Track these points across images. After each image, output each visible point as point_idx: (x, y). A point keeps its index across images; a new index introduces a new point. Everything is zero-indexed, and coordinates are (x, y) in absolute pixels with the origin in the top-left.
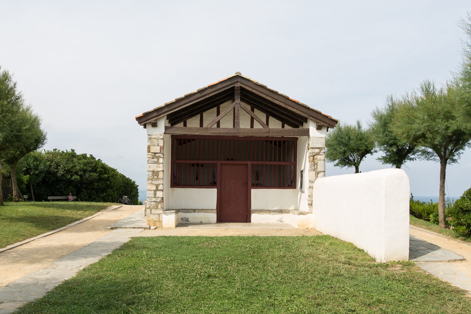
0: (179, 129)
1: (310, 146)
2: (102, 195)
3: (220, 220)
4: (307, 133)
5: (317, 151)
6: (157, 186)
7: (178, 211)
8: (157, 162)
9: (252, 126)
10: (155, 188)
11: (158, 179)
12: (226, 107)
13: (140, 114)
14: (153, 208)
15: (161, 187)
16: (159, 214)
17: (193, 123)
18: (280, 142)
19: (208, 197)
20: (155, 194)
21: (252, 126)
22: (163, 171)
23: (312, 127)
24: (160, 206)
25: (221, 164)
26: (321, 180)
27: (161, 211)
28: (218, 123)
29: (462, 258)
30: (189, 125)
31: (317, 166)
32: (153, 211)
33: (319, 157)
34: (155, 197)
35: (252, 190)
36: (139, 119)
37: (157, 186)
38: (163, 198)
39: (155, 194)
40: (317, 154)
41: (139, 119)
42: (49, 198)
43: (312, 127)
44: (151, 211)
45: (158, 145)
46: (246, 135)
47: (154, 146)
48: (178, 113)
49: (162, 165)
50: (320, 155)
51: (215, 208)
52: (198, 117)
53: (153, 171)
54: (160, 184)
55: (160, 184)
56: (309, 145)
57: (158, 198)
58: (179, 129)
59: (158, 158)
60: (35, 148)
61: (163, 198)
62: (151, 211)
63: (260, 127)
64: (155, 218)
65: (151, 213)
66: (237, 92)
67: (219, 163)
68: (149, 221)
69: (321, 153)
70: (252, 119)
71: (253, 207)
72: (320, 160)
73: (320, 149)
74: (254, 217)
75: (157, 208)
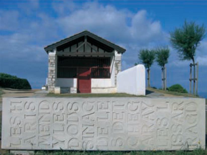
0: (61, 53)
1: (115, 60)
4: (114, 55)
5: (118, 62)
6: (53, 76)
8: (53, 66)
9: (92, 51)
11: (53, 73)
12: (81, 45)
13: (46, 46)
15: (54, 77)
16: (53, 88)
18: (103, 59)
20: (52, 80)
21: (92, 51)
23: (116, 53)
26: (120, 73)
27: (54, 87)
28: (77, 51)
29: (152, 124)
30: (72, 51)
32: (51, 87)
33: (119, 64)
37: (53, 76)
39: (52, 80)
40: (119, 63)
43: (116, 53)
47: (51, 59)
48: (61, 47)
52: (69, 48)
56: (114, 59)
58: (61, 53)
60: (174, 40)
63: (95, 52)
70: (92, 49)
73: (119, 61)
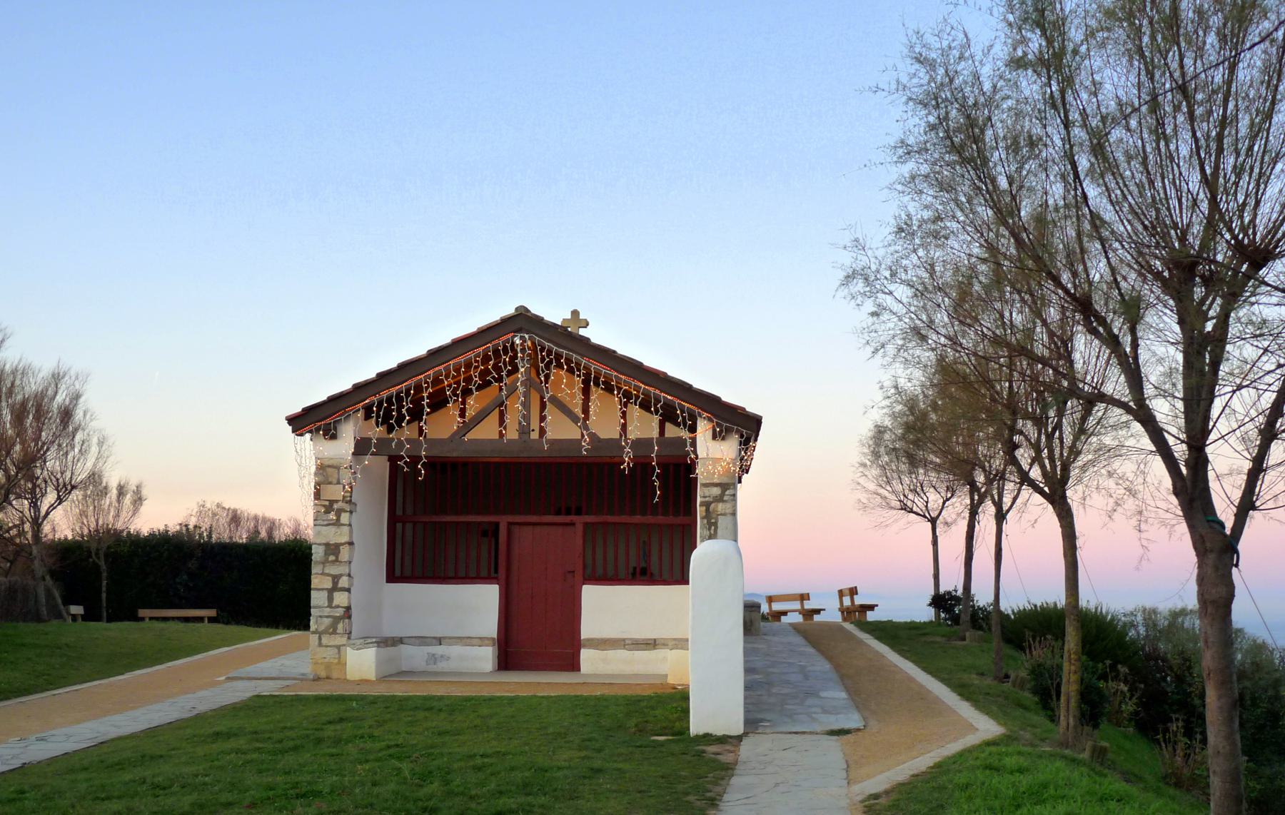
2: (966, 677)
3: (507, 661)
7: (387, 642)
8: (337, 523)
10: (329, 585)
13: (297, 409)
14: (325, 632)
15: (344, 582)
16: (338, 647)
17: (441, 426)
19: (478, 606)
20: (330, 599)
22: (351, 544)
24: (340, 626)
25: (510, 524)
31: (716, 528)
32: (325, 640)
34: (330, 606)
35: (585, 587)
36: (292, 420)
38: (348, 608)
39: (330, 599)
41: (292, 420)
42: (142, 613)
44: (320, 639)
45: (338, 483)
46: (564, 454)
48: (392, 400)
49: (346, 529)
50: (723, 501)
51: (495, 636)
53: (327, 545)
54: (341, 575)
55: (341, 575)
57: (338, 607)
59: (339, 513)
61: (348, 608)
62: (320, 639)
64: (329, 654)
65: (320, 645)
66: (526, 348)
67: (504, 521)
68: (316, 663)
69: (726, 498)
71: (586, 631)
72: (724, 514)
74: (586, 655)
75: (334, 632)
